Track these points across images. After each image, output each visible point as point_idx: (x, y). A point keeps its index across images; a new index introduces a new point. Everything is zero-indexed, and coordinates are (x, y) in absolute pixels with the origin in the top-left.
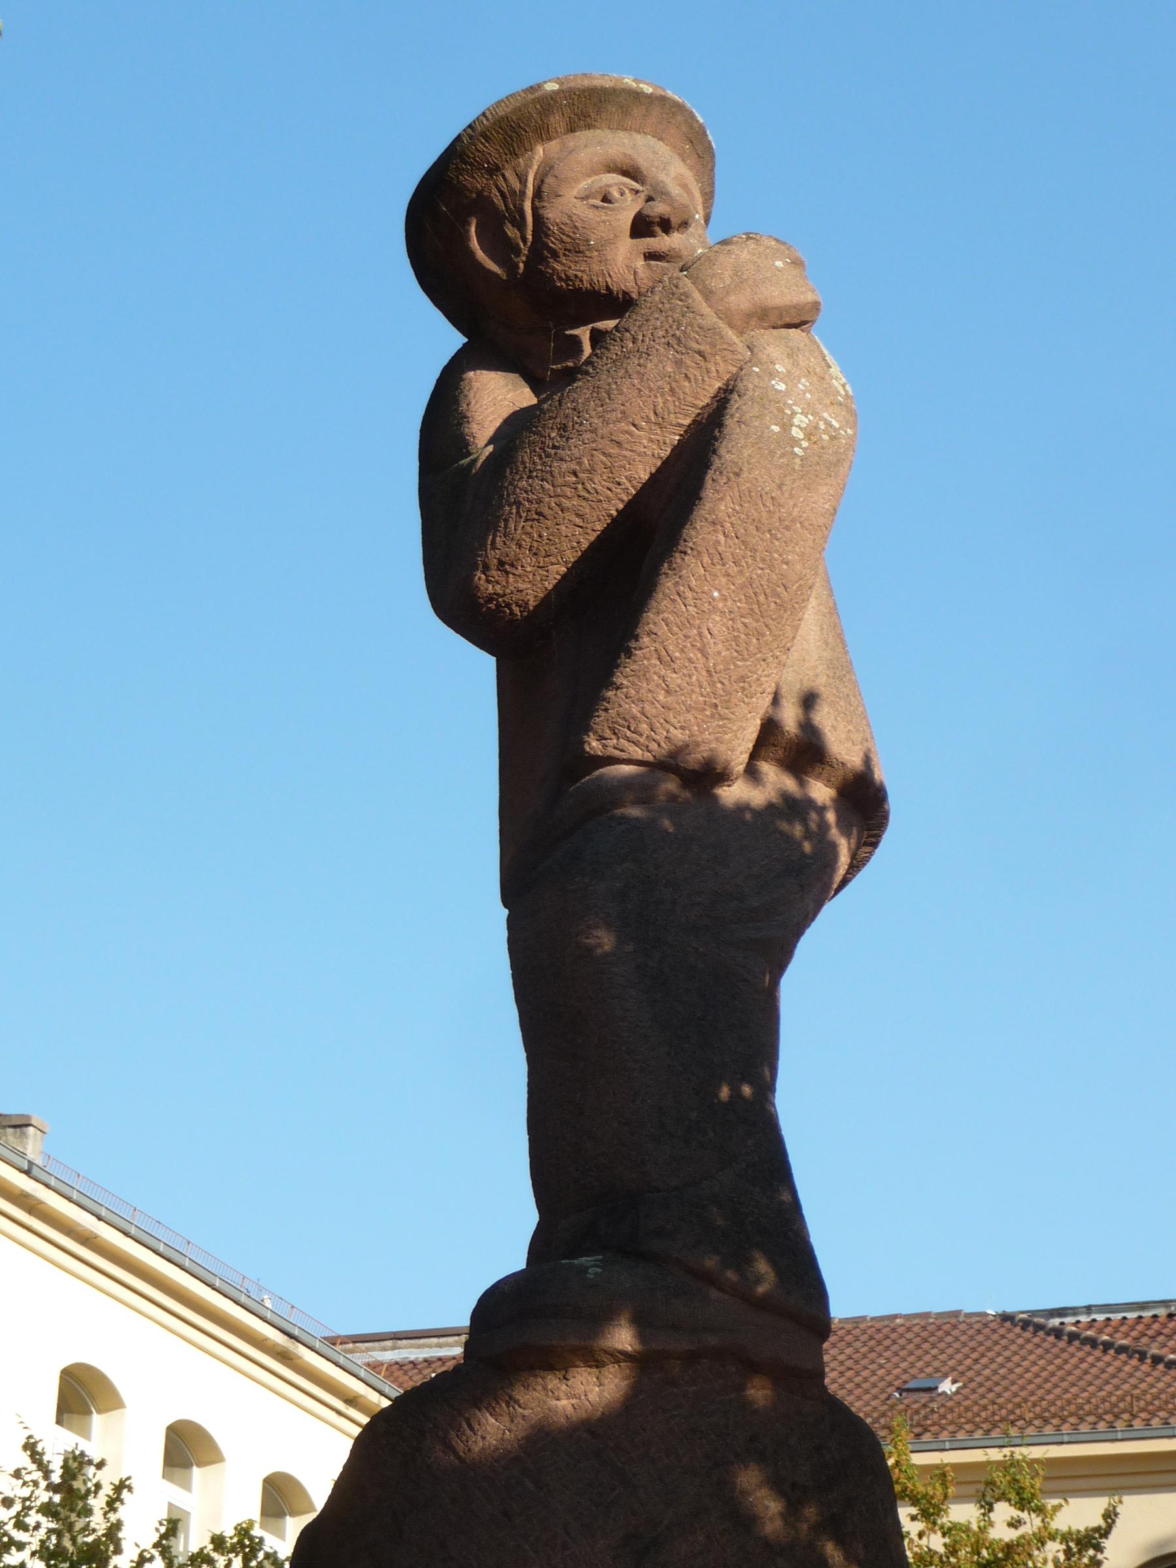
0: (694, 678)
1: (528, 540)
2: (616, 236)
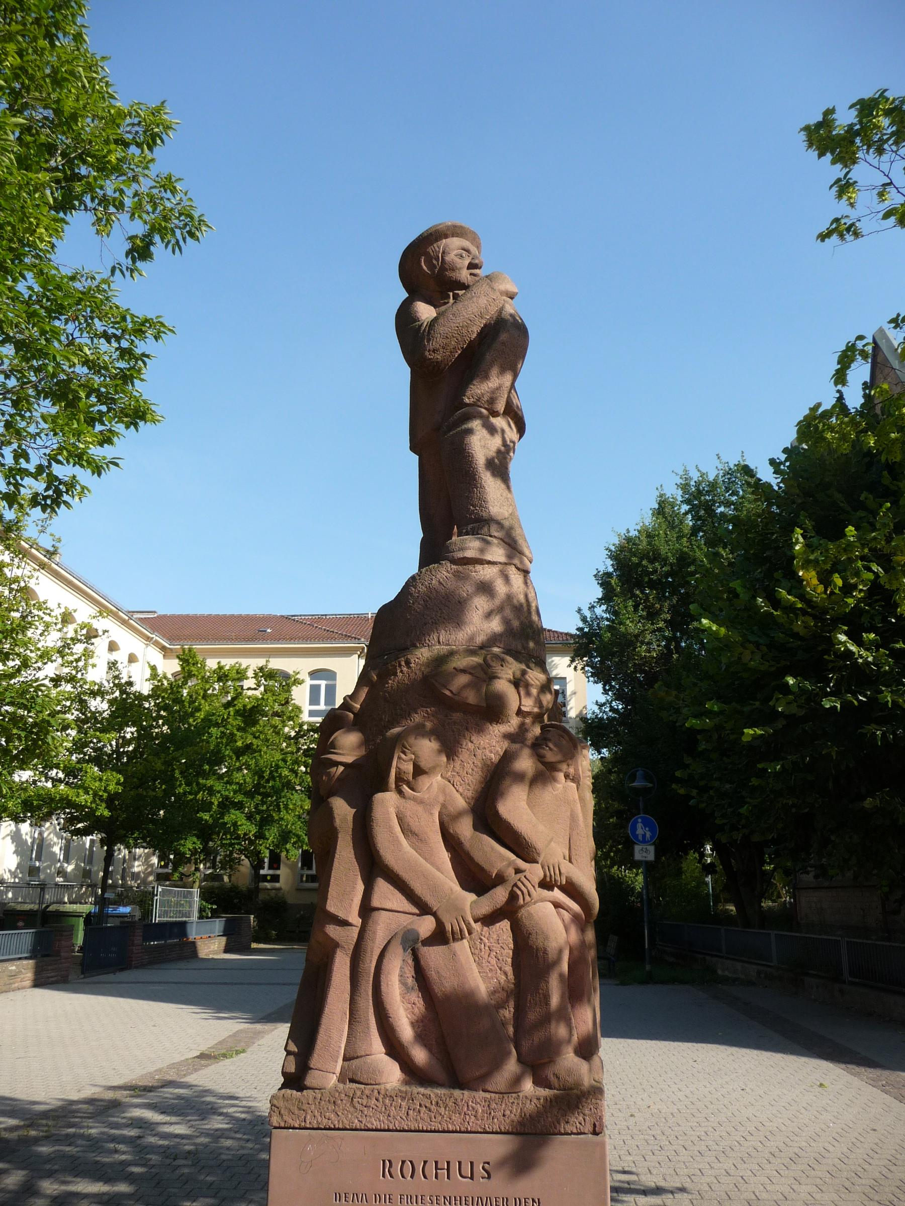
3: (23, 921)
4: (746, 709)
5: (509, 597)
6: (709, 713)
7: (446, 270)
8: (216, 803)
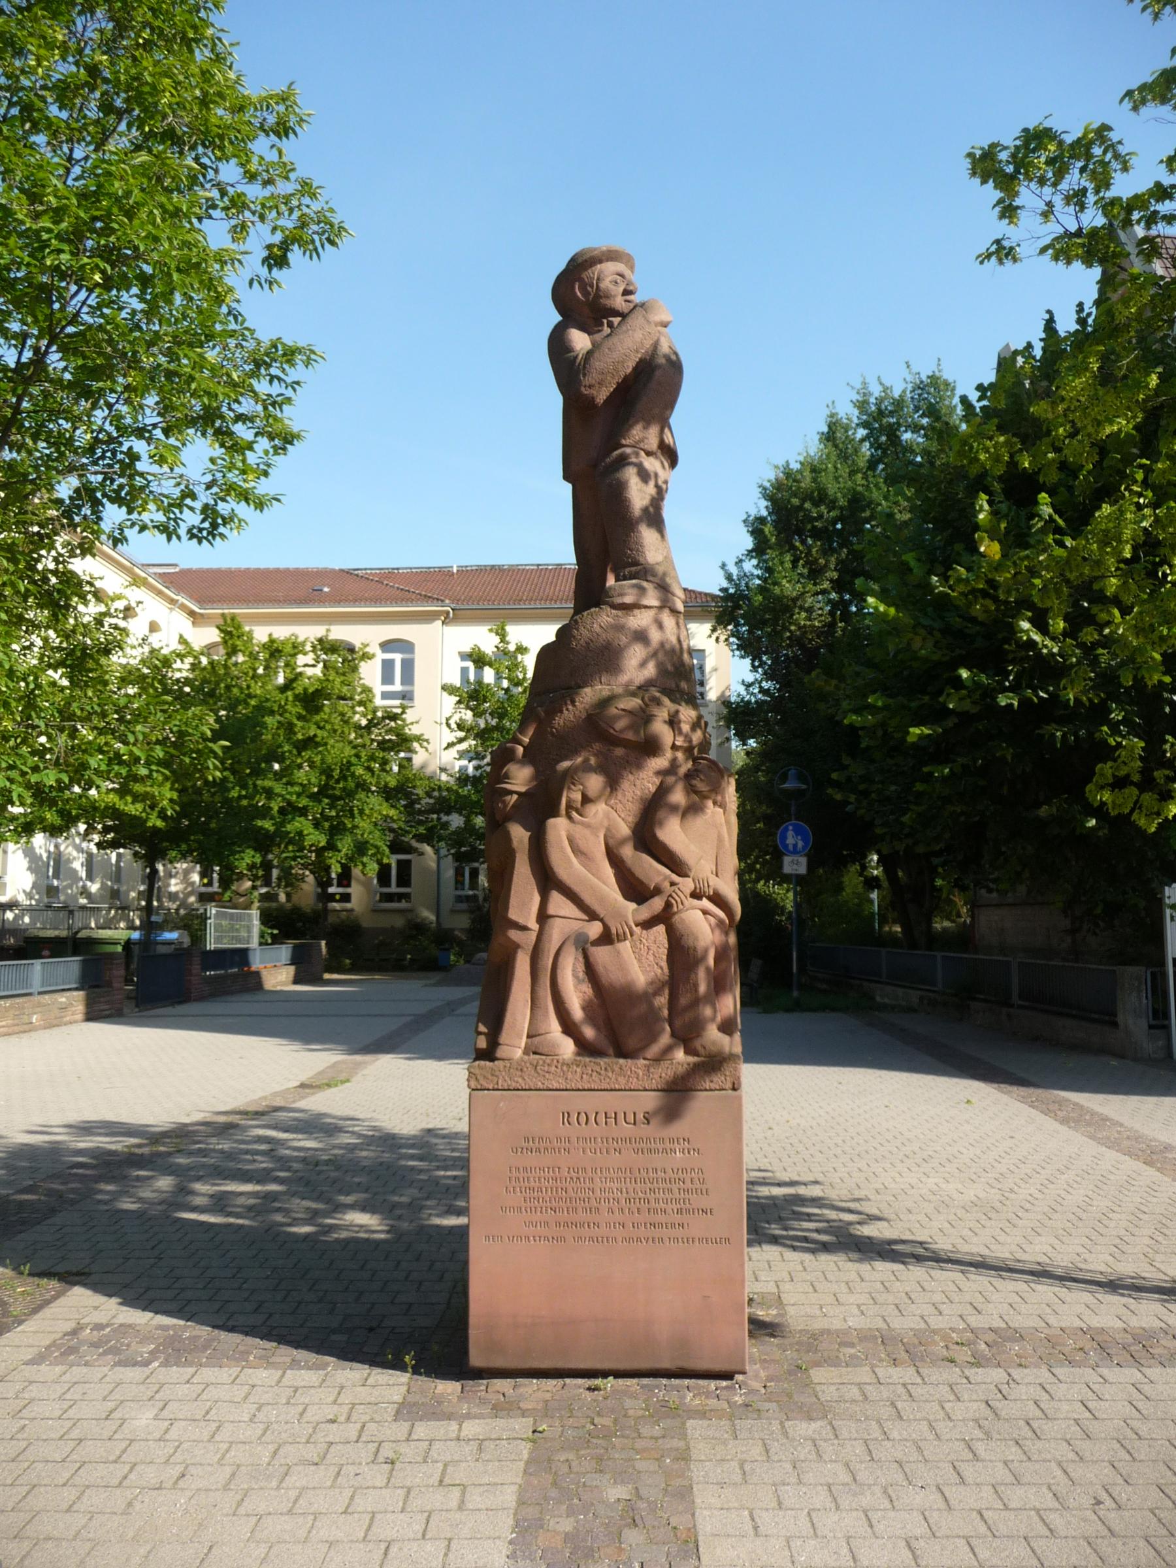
3: (49, 949)
4: (913, 704)
5: (662, 644)
6: (871, 708)
8: (276, 808)
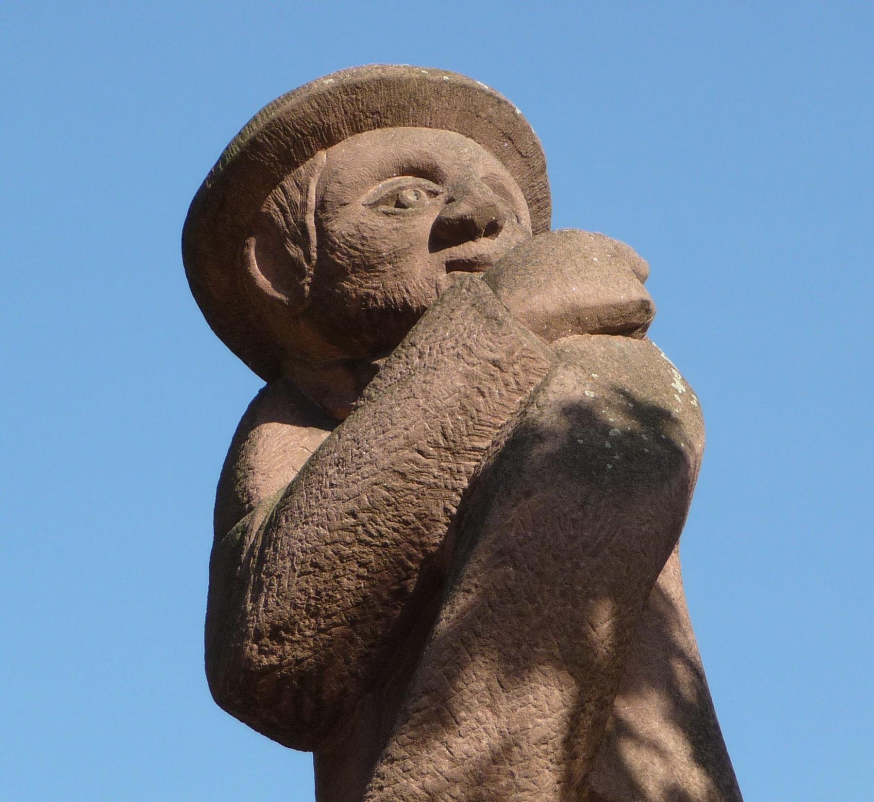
0: (485, 742)
1: (303, 597)
2: (411, 245)
7: (342, 273)
